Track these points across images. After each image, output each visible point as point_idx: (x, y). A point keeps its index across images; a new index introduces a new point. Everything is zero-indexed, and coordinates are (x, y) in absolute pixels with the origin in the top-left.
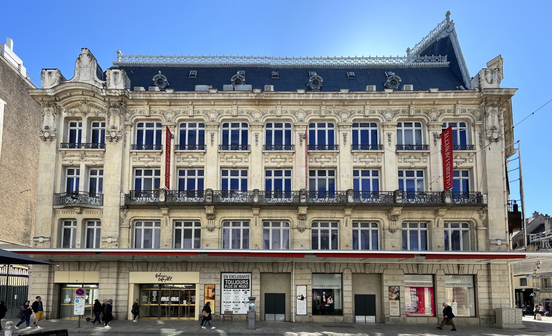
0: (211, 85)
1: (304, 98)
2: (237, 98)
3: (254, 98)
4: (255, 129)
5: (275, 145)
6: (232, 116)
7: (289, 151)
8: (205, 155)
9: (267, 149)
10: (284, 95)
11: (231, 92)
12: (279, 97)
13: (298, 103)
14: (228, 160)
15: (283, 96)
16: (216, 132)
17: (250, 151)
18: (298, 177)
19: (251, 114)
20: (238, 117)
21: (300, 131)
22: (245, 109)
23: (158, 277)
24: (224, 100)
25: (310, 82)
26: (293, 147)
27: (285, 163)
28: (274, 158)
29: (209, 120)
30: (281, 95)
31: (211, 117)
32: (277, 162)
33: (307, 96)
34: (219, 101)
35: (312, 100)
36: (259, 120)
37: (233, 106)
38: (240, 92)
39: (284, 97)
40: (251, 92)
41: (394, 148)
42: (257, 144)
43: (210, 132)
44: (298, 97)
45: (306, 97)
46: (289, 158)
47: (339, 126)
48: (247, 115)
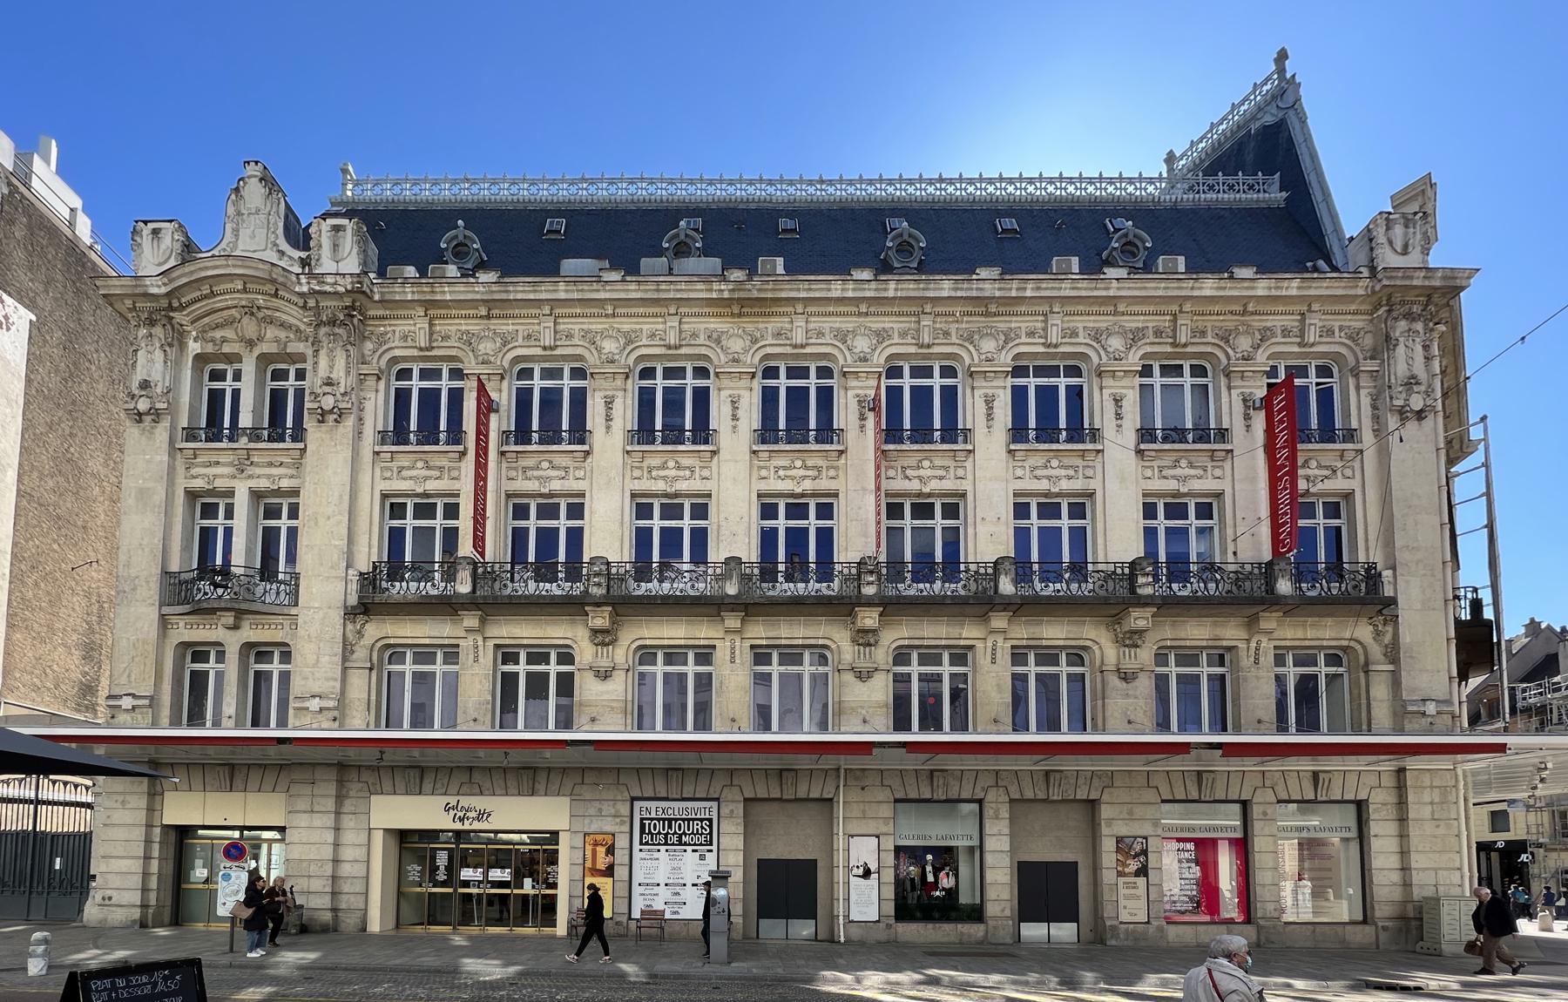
3: (726, 295)
4: (732, 385)
5: (788, 430)
7: (827, 447)
8: (589, 460)
10: (1044, 285)
11: (661, 279)
14: (654, 473)
15: (810, 289)
16: (620, 394)
19: (718, 341)
20: (683, 351)
21: (861, 388)
22: (702, 326)
23: (452, 813)
25: (890, 248)
28: (785, 468)
29: (600, 358)
30: (806, 287)
32: (792, 478)
35: (894, 298)
36: (742, 357)
37: (667, 318)
38: (686, 278)
41: (1130, 438)
43: (602, 394)
46: (828, 468)
47: (971, 374)
48: (708, 343)
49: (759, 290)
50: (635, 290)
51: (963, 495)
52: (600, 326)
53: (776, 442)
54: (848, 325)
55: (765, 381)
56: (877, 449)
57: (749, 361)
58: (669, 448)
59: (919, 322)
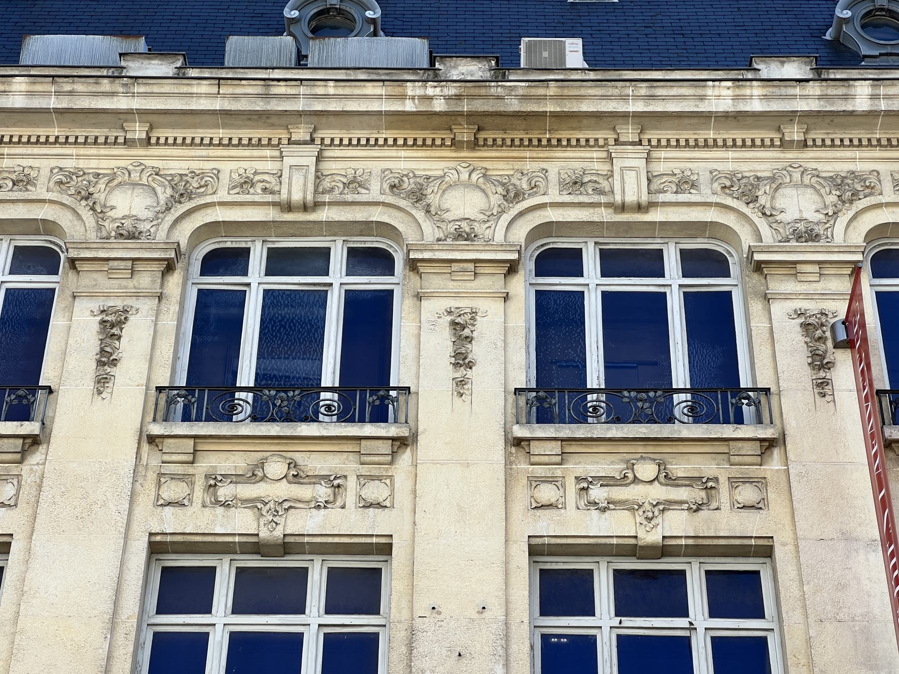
0: (138, 35)
1: (814, 106)
2: (318, 106)
3: (439, 106)
4: (452, 286)
5: (612, 389)
6: (274, 204)
7: (727, 431)
8: (36, 458)
9: (544, 417)
10: (660, 92)
11: (277, 74)
12: (624, 98)
13: (769, 135)
14: (225, 492)
15: (652, 97)
16: (146, 306)
17: (404, 432)
18: (829, 627)
19: (418, 196)
20: (324, 215)
21: (808, 296)
22: (377, 167)
24: (227, 117)
25: (846, 21)
26: (758, 404)
27: (704, 514)
28: (607, 481)
29: (99, 227)
30: (643, 92)
31: (117, 213)
32: (633, 507)
33: (831, 91)
34: (189, 119)
35: (872, 114)
36: (479, 229)
37: (286, 150)
38: (341, 75)
39: (664, 98)
40: (421, 75)
42: (461, 383)
43: (95, 305)
44: (765, 98)
45: (820, 98)
46: (734, 482)
47: (759, 267)
48: (390, 199)
49: (525, 98)
50: (208, 95)
51: (766, 551)
52: (113, 164)
53: (581, 418)
54: (762, 167)
55: (541, 280)
56: (870, 438)
57: (499, 237)
58: (274, 429)
59: (610, 159)
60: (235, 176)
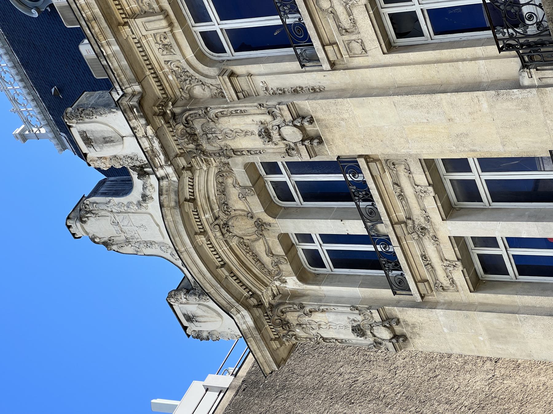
60: (165, 53)
